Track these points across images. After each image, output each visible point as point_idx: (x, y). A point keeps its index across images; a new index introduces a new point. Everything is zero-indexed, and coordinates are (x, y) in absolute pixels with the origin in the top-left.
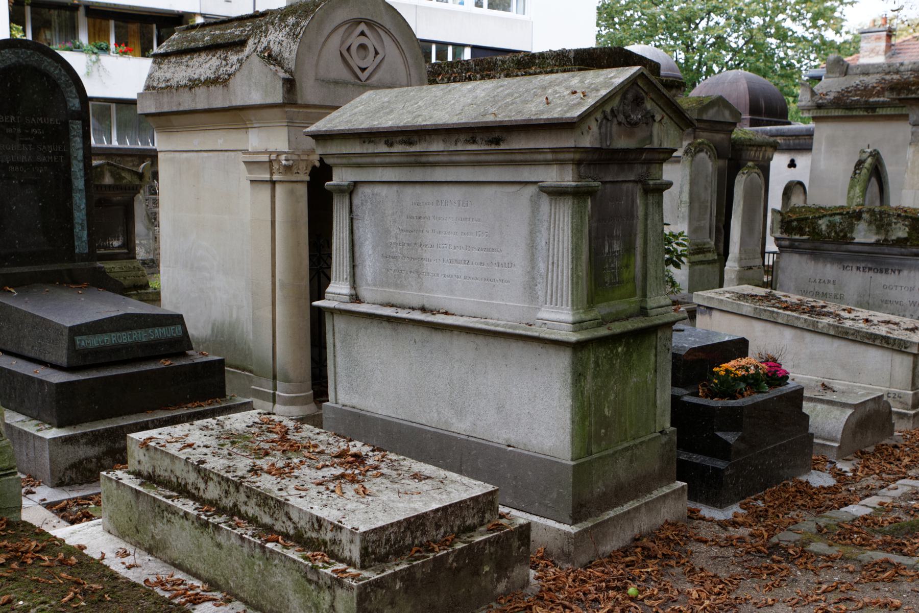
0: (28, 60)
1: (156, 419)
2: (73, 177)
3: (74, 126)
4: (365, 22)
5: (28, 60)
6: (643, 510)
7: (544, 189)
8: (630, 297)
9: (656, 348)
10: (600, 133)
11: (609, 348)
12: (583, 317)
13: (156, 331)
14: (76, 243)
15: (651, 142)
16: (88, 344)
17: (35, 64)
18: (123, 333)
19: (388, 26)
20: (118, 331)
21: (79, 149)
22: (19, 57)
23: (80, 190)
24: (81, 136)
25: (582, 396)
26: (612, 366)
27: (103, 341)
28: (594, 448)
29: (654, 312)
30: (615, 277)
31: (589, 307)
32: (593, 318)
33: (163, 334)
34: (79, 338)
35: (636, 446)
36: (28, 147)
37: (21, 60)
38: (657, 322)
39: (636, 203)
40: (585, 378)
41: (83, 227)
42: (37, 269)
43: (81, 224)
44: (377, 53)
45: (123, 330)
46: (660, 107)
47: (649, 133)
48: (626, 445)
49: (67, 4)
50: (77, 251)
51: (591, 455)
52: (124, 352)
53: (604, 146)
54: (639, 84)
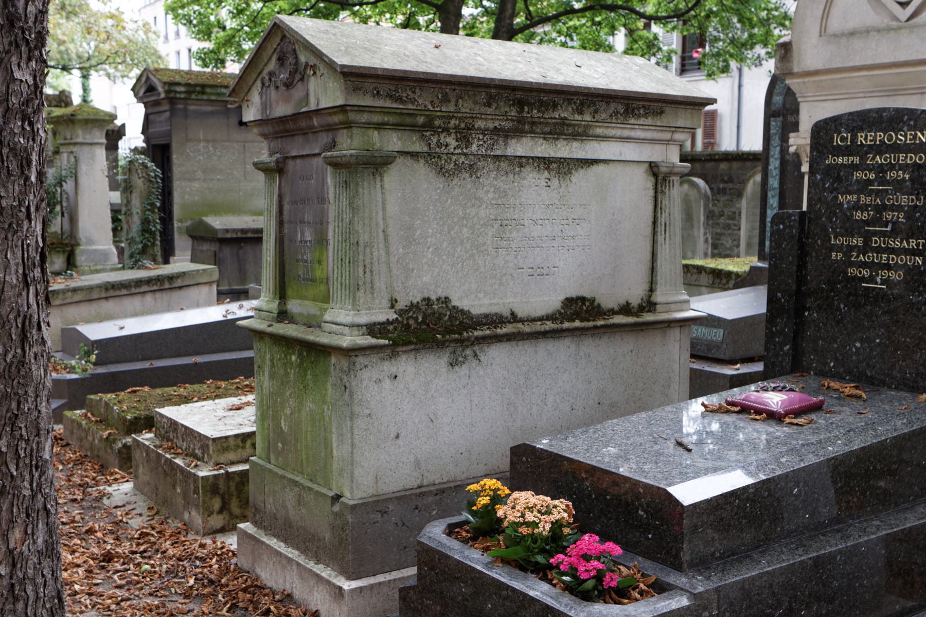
7: (260, 166)
13: (700, 330)
15: (307, 104)
23: (775, 188)
26: (287, 374)
29: (327, 327)
30: (308, 273)
32: (269, 310)
39: (327, 183)
47: (305, 93)
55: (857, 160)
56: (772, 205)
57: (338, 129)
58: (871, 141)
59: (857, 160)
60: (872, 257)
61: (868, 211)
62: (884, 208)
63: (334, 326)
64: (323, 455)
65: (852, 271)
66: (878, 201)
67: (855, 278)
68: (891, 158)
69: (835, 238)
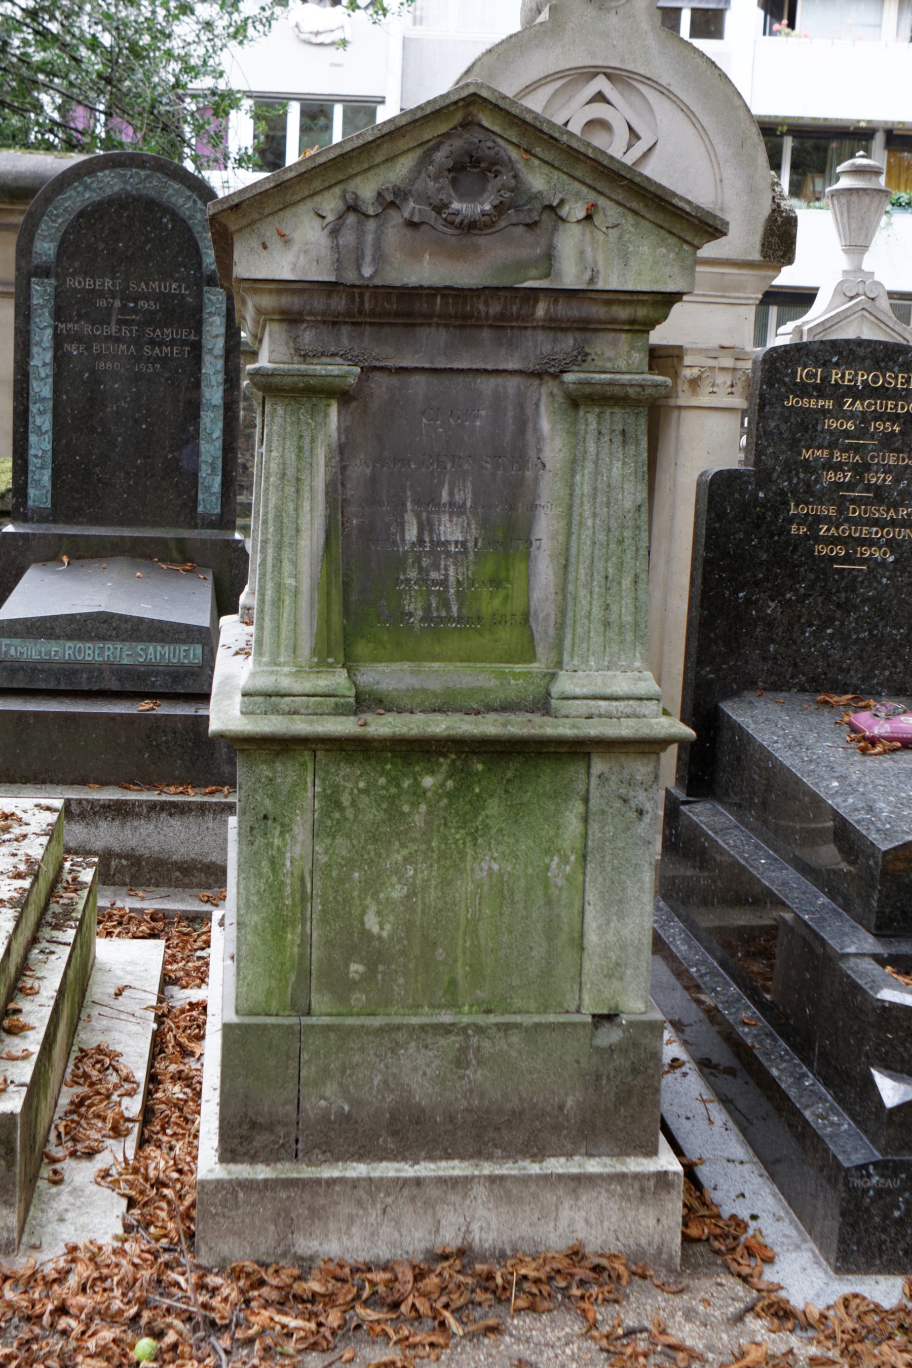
0: (140, 186)
1: (87, 800)
2: (203, 384)
3: (212, 297)
4: (605, 74)
5: (140, 186)
6: (480, 1191)
8: (510, 659)
9: (586, 800)
10: (336, 248)
11: (383, 773)
12: (286, 683)
13: (151, 650)
14: (200, 497)
16: (22, 654)
17: (153, 194)
18: (88, 645)
19: (665, 79)
20: (80, 638)
21: (217, 336)
22: (126, 182)
23: (215, 406)
24: (224, 313)
25: (274, 870)
27: (48, 653)
28: (320, 1001)
31: (319, 664)
32: (326, 690)
33: (162, 656)
34: (8, 641)
35: (480, 1030)
36: (131, 331)
37: (129, 188)
38: (593, 729)
39: (537, 429)
40: (286, 829)
41: (214, 469)
42: (127, 532)
43: (212, 464)
44: (634, 135)
45: (91, 639)
46: (583, 183)
48: (446, 1018)
49: (848, 128)
50: (200, 509)
51: (309, 1013)
52: (85, 676)
53: (350, 277)
54: (486, 124)
55: (829, 404)
56: (40, 427)
57: (596, 330)
58: (850, 381)
59: (829, 404)
60: (845, 530)
61: (844, 471)
62: (867, 467)
63: (602, 703)
64: (538, 952)
65: (822, 550)
66: (857, 458)
67: (822, 559)
68: (878, 405)
69: (797, 506)
